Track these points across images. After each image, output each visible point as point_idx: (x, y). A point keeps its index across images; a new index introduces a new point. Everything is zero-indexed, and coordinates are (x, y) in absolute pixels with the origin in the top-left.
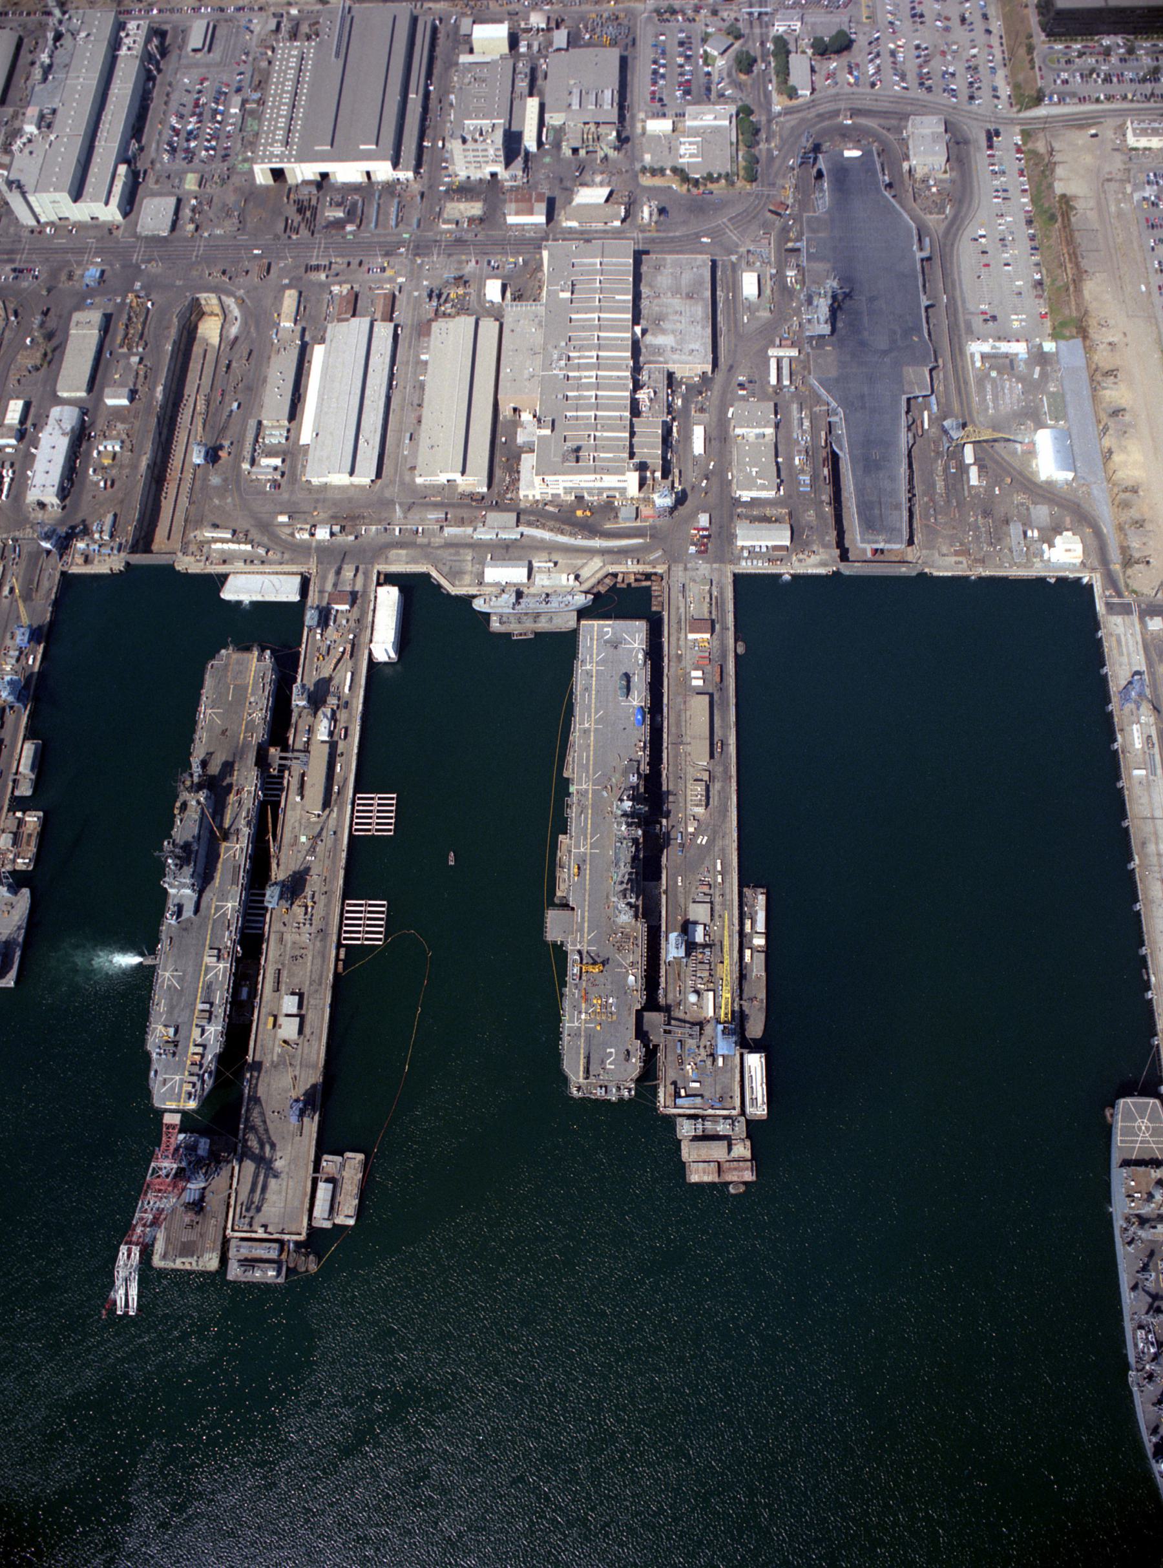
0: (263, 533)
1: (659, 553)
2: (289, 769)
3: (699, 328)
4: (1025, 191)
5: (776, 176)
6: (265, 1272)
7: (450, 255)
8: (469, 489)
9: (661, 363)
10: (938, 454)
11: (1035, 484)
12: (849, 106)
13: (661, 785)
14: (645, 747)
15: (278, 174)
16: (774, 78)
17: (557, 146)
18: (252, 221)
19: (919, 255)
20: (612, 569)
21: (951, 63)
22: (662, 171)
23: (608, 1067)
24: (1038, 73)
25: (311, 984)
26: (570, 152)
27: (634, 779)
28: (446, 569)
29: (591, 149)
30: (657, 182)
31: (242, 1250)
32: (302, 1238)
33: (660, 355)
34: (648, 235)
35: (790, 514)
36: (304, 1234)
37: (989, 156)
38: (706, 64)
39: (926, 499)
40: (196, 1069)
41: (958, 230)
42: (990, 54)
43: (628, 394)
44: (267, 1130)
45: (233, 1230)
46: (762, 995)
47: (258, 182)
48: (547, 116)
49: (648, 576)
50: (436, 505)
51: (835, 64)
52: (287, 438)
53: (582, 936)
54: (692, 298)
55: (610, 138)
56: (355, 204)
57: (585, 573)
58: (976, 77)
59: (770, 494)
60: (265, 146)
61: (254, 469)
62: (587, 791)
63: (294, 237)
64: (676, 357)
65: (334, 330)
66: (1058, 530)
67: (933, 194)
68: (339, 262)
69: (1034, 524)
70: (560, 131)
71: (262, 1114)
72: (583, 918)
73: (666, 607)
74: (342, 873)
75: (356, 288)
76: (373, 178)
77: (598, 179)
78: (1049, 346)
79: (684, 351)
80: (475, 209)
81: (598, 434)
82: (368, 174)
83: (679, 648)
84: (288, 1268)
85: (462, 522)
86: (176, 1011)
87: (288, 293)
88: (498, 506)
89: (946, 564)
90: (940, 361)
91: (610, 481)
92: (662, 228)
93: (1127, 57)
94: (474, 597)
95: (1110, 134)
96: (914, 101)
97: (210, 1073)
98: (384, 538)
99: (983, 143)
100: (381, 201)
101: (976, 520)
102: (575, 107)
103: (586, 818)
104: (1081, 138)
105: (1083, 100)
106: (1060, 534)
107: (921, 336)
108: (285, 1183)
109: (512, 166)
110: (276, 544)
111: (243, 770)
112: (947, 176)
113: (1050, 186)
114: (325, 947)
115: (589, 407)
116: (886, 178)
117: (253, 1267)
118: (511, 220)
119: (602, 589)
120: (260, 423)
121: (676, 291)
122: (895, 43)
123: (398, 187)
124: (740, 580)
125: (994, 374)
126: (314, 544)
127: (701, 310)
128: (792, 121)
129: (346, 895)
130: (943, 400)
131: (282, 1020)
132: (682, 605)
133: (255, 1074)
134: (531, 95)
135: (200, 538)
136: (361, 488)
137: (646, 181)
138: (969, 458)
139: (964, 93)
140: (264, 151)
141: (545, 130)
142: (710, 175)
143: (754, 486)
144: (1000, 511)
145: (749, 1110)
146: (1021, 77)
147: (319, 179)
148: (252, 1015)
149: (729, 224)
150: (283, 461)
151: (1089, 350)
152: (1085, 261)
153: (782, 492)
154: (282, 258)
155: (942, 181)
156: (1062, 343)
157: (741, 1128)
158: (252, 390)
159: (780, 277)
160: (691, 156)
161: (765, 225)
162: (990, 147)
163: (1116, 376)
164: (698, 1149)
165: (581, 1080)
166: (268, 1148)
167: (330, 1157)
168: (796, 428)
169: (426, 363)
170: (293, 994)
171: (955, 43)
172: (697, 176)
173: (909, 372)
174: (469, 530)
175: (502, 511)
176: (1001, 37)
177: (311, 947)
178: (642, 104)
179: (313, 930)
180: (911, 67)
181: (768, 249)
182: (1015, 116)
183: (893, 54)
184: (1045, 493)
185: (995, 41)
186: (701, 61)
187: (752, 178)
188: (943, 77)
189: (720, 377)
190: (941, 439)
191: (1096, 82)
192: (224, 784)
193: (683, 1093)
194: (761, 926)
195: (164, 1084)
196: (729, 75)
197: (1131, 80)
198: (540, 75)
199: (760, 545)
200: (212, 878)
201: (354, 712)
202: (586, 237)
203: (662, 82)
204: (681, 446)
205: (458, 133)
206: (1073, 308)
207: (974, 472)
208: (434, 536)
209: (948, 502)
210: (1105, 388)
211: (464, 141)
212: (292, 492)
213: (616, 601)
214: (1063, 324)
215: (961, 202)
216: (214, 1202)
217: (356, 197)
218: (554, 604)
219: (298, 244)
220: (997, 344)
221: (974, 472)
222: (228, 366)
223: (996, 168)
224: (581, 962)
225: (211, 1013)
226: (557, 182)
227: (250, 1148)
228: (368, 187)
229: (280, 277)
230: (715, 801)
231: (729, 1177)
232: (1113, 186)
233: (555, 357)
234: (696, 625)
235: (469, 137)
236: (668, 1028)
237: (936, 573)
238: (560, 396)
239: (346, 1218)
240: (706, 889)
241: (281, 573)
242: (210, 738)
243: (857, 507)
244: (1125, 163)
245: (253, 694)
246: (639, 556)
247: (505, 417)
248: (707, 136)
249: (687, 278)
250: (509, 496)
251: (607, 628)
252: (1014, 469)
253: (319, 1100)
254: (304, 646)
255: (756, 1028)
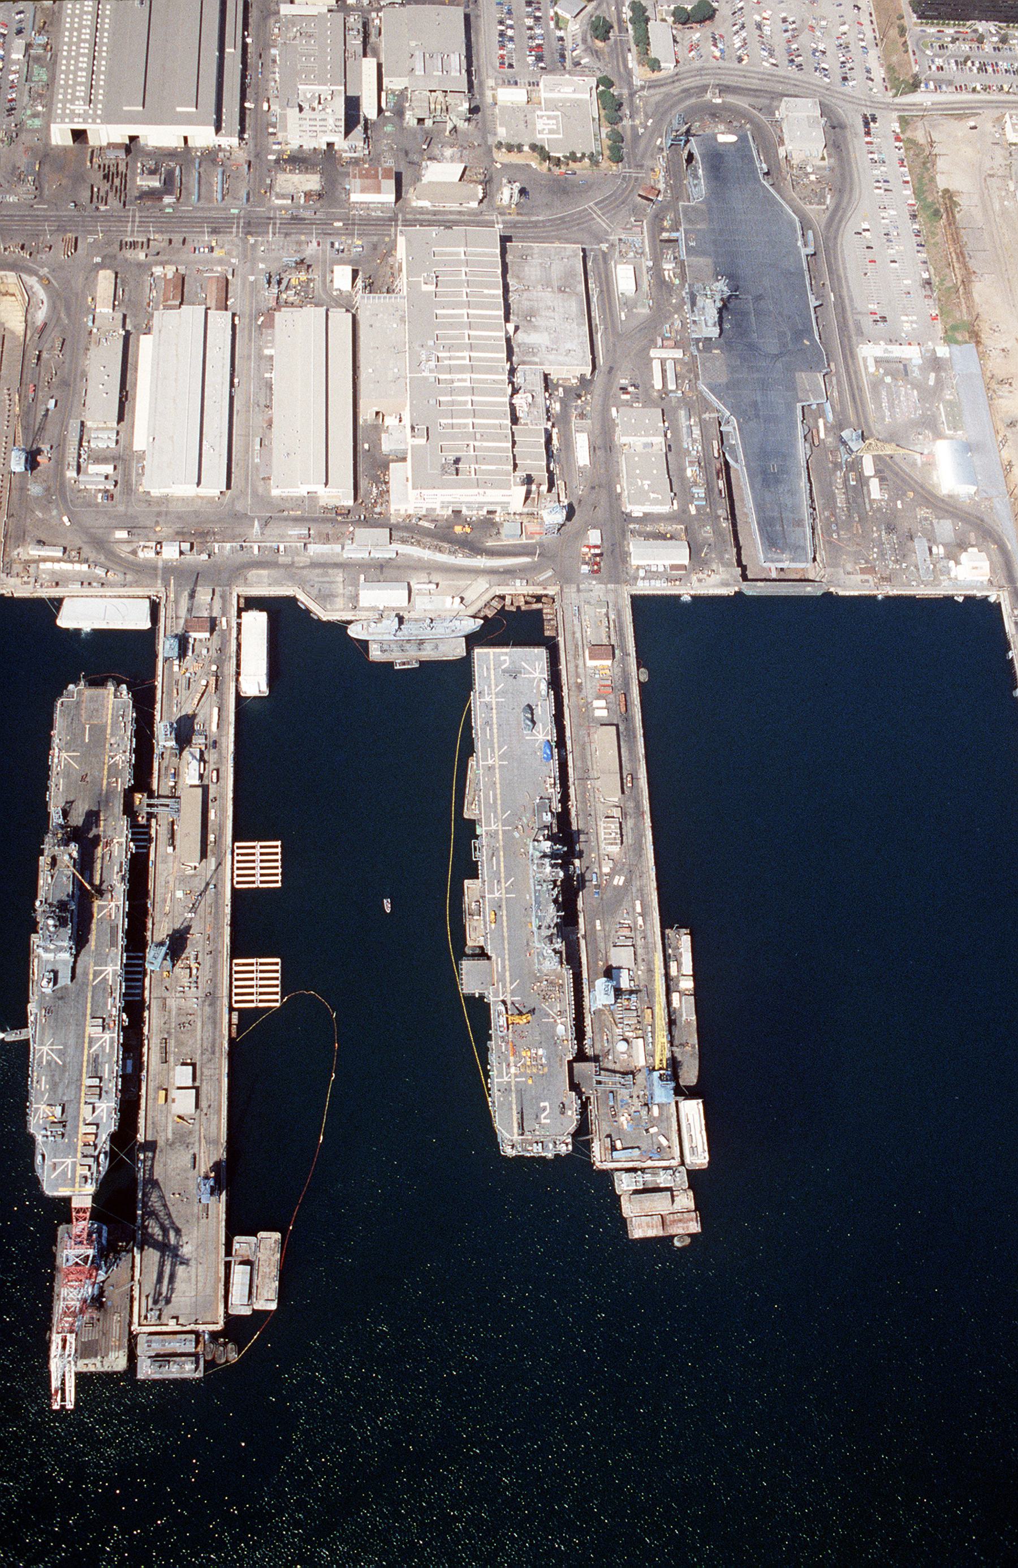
0: (98, 552)
1: (550, 573)
2: (156, 817)
3: (574, 325)
4: (907, 182)
5: (643, 157)
6: (181, 1365)
7: (287, 235)
8: (332, 503)
9: (536, 364)
10: (837, 466)
11: (935, 497)
12: (717, 82)
13: (570, 824)
14: (555, 784)
15: (79, 135)
16: (634, 48)
17: (400, 113)
18: (50, 188)
19: (804, 251)
20: (500, 591)
21: (819, 40)
22: (519, 148)
23: (543, 1121)
24: (912, 58)
25: (202, 1054)
26: (416, 121)
27: (547, 818)
28: (314, 592)
29: (438, 119)
30: (514, 158)
31: (154, 1345)
32: (219, 1327)
33: (534, 354)
34: (507, 218)
35: (686, 528)
36: (222, 1323)
37: (867, 143)
38: (558, 27)
39: (826, 513)
40: (90, 1151)
41: (840, 222)
42: (860, 33)
43: (507, 399)
44: (169, 1215)
45: (140, 1325)
46: (694, 1040)
47: (54, 142)
48: (385, 80)
49: (538, 599)
50: (296, 520)
51: (698, 35)
52: (117, 442)
53: (504, 986)
54: (564, 292)
55: (460, 109)
56: (170, 174)
57: (470, 595)
58: (848, 55)
59: (664, 509)
60: (64, 102)
61: (81, 478)
62: (496, 832)
63: (102, 208)
64: (551, 357)
65: (164, 319)
66: (962, 545)
67: (812, 182)
68: (159, 239)
69: (939, 540)
70: (402, 95)
71: (162, 1197)
72: (504, 967)
73: (561, 631)
74: (227, 930)
75: (182, 270)
76: (190, 144)
77: (448, 152)
78: (943, 351)
79: (561, 350)
80: (312, 182)
81: (477, 444)
82: (186, 139)
83: (578, 676)
84: (205, 1361)
85: (327, 539)
86: (60, 1091)
87: (102, 273)
88: (368, 522)
89: (852, 583)
90: (832, 365)
91: (493, 496)
92: (525, 211)
93: (1000, 46)
94: (350, 622)
95: (989, 127)
96: (784, 80)
97: (105, 1153)
98: (243, 557)
99: (861, 129)
100: (202, 170)
101: (880, 536)
102: (419, 72)
103: (498, 863)
104: (961, 129)
105: (959, 89)
106: (966, 550)
107: (812, 340)
108: (194, 1270)
109: (350, 136)
110: (117, 563)
111: (110, 819)
112: (825, 163)
113: (932, 179)
114: (215, 1012)
115: (464, 414)
116: (764, 166)
117: (169, 1362)
118: (355, 197)
119: (490, 613)
120: (82, 424)
121: (548, 284)
122: (760, 15)
123: (221, 155)
124: (639, 603)
125: (888, 379)
126: (160, 564)
127: (574, 306)
128: (656, 95)
129: (234, 955)
130: (838, 408)
131: (174, 1093)
132: (577, 629)
133: (150, 1155)
134: (365, 55)
135: (24, 557)
136: (210, 500)
137: (502, 157)
138: (869, 468)
139: (837, 73)
140: (64, 108)
141: (383, 94)
142: (573, 154)
143: (645, 495)
144: (904, 525)
145: (688, 1160)
146: (894, 59)
147: (128, 142)
148: (140, 1089)
149: (595, 208)
150: (115, 468)
151: (982, 356)
152: (973, 260)
153: (676, 507)
154: (90, 233)
155: (819, 168)
156: (955, 348)
157: (682, 1179)
158: (70, 384)
159: (657, 271)
160: (551, 132)
161: (635, 211)
162: (868, 133)
163: (1010, 384)
164: (641, 1201)
165: (516, 1138)
166: (172, 1234)
167: (243, 1238)
168: (685, 437)
169: (271, 357)
170: (184, 1064)
171: (824, 19)
172: (560, 155)
173: (803, 378)
174: (337, 548)
175: (372, 527)
176: (871, 15)
177: (199, 1013)
178: (490, 73)
179: (200, 993)
180: (779, 41)
181: (642, 238)
182: (890, 100)
183: (759, 26)
184: (946, 507)
185: (865, 20)
186: (552, 24)
187: (618, 159)
188: (814, 54)
189: (600, 379)
190: (838, 450)
191: (971, 70)
192: (91, 836)
193: (619, 1145)
194: (688, 967)
195: (55, 1169)
196: (584, 41)
197: (1006, 71)
198: (373, 32)
199: (659, 566)
200: (87, 941)
201: (224, 752)
202: (446, 222)
203: (510, 46)
204: (563, 455)
205: (294, 102)
206: (965, 310)
207: (874, 484)
208: (298, 555)
209: (850, 516)
210: (1001, 397)
211: (301, 109)
212: (128, 503)
213: (514, 626)
214: (954, 328)
215: (841, 191)
216: (114, 1297)
217: (172, 164)
218: (440, 630)
219: (106, 217)
220: (890, 347)
221: (874, 484)
222: (39, 357)
223: (875, 156)
224: (507, 1012)
225: (101, 1088)
226: (402, 155)
227: (152, 1236)
228: (184, 154)
229: (90, 255)
230: (629, 839)
231: (673, 1230)
232: (994, 183)
233: (424, 357)
234: (598, 650)
235: (306, 106)
236: (599, 1078)
237: (841, 593)
238: (432, 402)
239: (268, 1302)
240: (627, 932)
241: (124, 597)
242: (68, 787)
243: (758, 524)
244: (1006, 159)
245: (112, 735)
246: (528, 577)
247: (365, 421)
248: (568, 109)
249: (557, 270)
250: (377, 510)
251: (503, 656)
252: (916, 482)
253: (227, 1177)
254: (160, 679)
255: (690, 1076)
